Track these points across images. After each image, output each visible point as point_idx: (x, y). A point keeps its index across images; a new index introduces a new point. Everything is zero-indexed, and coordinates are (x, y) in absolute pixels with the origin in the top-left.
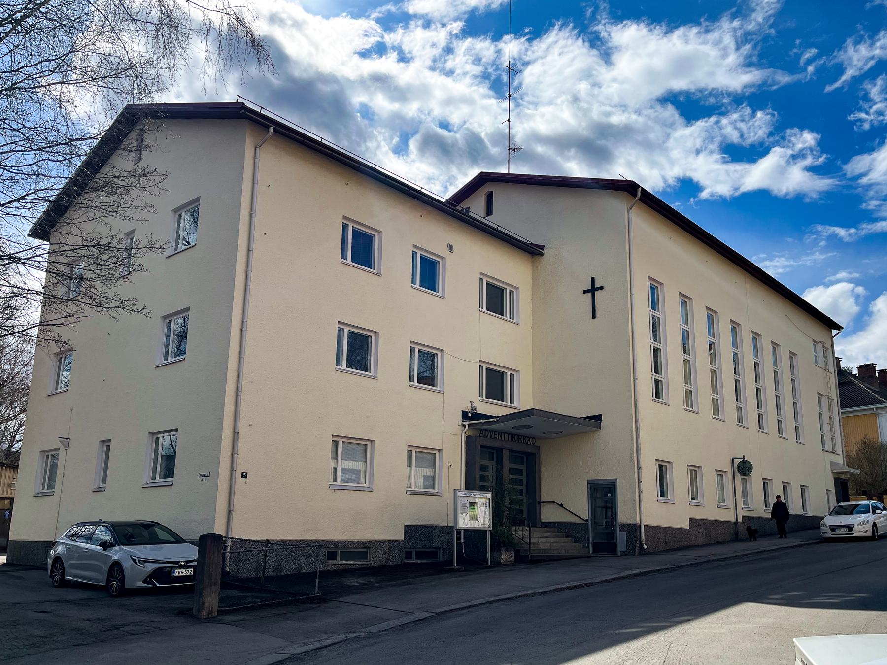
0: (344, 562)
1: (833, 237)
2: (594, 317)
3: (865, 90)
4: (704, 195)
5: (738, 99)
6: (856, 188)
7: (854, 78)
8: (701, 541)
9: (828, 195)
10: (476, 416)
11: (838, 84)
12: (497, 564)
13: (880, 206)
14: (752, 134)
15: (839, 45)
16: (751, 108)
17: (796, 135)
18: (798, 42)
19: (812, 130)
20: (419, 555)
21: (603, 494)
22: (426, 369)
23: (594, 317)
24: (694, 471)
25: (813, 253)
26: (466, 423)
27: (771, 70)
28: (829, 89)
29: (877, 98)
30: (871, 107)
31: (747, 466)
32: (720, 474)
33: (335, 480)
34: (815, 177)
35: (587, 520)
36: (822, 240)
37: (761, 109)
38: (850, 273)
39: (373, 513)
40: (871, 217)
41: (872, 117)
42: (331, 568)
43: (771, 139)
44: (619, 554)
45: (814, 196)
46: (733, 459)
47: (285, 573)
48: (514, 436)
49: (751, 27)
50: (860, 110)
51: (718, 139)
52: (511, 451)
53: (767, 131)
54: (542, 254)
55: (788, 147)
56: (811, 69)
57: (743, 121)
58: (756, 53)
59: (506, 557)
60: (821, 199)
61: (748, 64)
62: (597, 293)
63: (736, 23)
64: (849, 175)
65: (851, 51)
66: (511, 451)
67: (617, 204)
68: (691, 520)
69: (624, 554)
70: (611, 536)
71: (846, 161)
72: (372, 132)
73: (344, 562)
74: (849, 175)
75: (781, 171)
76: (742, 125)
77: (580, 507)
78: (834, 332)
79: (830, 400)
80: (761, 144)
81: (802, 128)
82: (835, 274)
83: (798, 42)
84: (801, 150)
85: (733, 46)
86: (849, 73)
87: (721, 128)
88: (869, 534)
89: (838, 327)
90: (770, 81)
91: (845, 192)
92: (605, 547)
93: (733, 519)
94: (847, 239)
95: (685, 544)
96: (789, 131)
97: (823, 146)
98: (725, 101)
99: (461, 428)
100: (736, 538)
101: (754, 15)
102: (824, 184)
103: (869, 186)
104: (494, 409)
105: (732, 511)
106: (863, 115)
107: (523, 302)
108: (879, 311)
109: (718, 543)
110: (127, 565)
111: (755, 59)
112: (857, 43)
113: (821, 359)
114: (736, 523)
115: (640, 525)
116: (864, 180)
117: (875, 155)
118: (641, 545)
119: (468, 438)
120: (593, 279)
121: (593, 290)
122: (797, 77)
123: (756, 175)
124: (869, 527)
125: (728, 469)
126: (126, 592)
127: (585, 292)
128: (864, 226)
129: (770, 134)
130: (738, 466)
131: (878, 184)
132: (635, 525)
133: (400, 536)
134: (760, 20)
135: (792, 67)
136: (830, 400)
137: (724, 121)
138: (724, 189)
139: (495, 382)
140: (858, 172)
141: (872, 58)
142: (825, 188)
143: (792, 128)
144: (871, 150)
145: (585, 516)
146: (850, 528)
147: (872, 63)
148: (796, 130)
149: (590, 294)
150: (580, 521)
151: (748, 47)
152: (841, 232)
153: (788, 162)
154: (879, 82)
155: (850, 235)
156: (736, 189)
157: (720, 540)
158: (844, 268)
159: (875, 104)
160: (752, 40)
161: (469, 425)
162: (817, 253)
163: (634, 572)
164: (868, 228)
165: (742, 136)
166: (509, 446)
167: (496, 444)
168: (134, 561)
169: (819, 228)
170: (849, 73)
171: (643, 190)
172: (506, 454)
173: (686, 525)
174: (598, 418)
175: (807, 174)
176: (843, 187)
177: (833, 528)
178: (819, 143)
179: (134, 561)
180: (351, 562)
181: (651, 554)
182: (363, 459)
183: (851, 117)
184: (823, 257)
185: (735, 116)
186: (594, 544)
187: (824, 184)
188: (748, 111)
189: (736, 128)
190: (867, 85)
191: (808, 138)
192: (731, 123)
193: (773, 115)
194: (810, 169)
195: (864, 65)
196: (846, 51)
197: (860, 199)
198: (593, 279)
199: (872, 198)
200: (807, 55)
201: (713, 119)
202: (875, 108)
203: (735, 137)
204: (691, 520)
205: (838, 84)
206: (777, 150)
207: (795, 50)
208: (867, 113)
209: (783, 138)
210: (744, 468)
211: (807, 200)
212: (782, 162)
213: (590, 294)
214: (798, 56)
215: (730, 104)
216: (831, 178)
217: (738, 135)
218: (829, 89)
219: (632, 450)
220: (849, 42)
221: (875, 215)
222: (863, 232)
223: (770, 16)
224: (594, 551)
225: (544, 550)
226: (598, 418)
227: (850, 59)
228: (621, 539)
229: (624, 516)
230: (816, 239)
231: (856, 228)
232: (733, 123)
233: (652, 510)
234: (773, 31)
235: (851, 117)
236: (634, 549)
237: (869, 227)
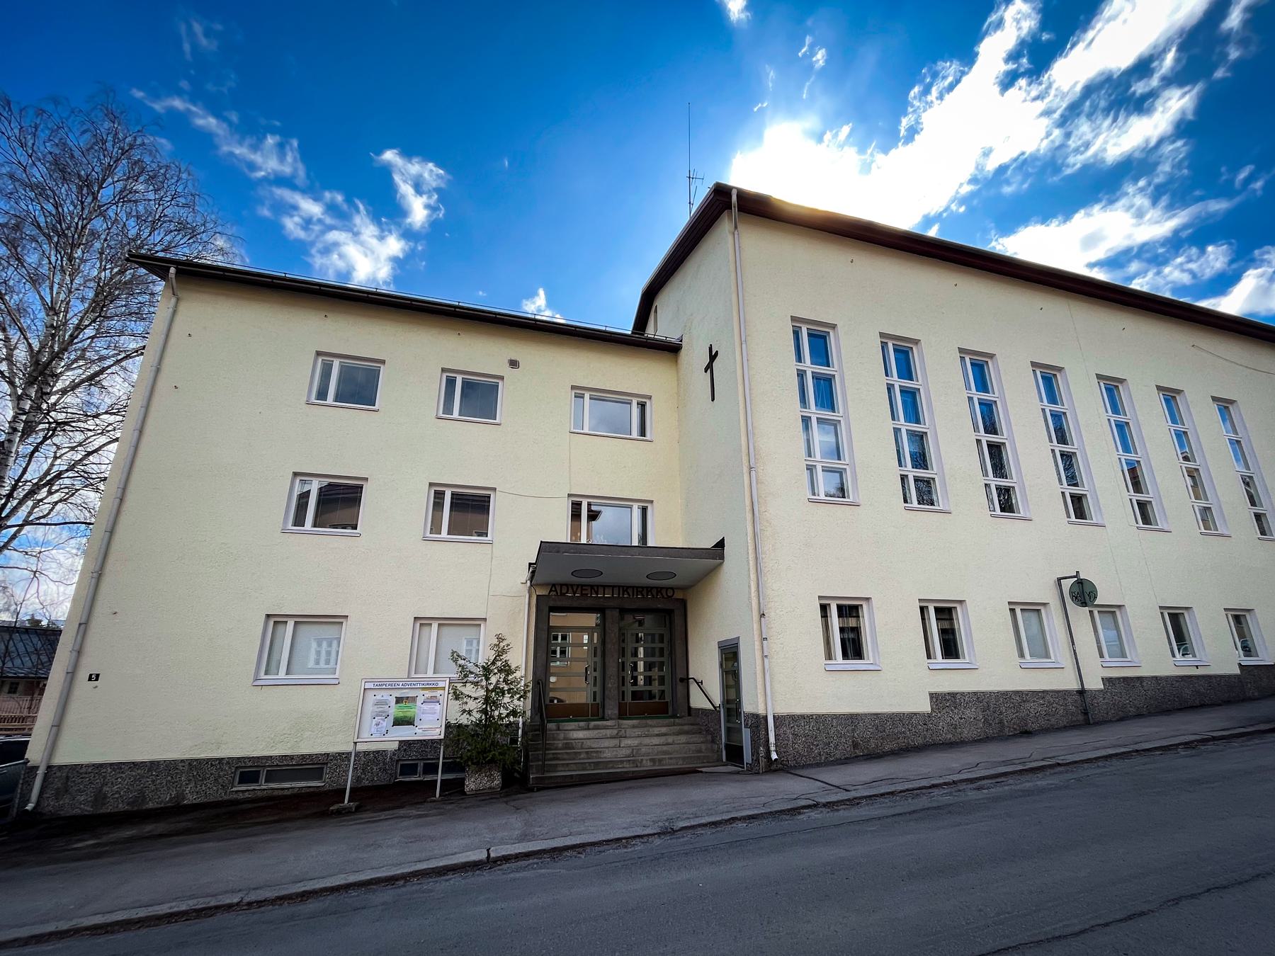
0: (243, 788)
18: (1223, 169)
31: (1087, 590)
39: (341, 711)
42: (241, 796)
46: (1059, 580)
49: (1157, 180)
68: (932, 695)
73: (243, 788)
76: (1193, 266)
93: (1075, 686)
98: (1161, 251)
109: (1027, 733)
114: (1082, 692)
115: (766, 718)
118: (768, 752)
129: (1232, 262)
137: (1167, 270)
157: (1029, 728)
173: (925, 707)
182: (328, 631)
185: (1179, 260)
200: (1243, 175)
204: (932, 695)
207: (1224, 178)
214: (1232, 181)
215: (1167, 252)
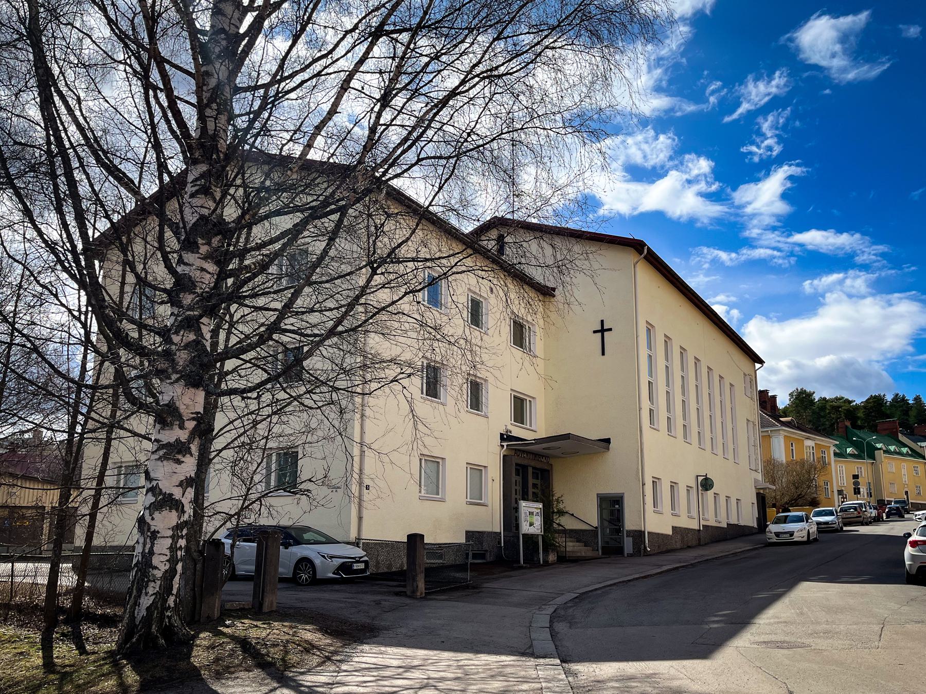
1: (715, 261)
2: (603, 354)
3: (758, 124)
4: (601, 212)
5: (644, 122)
6: (743, 216)
7: (749, 111)
8: (678, 546)
9: (718, 221)
11: (735, 116)
12: (546, 563)
13: (761, 234)
14: (654, 156)
15: (742, 81)
16: (656, 132)
17: (693, 161)
18: (706, 73)
19: (709, 157)
20: (475, 556)
21: (612, 506)
22: (476, 395)
23: (603, 354)
24: (673, 486)
25: (697, 276)
26: (505, 444)
27: (678, 98)
28: (727, 119)
29: (769, 134)
30: (762, 142)
33: (420, 492)
34: (708, 203)
36: (706, 262)
37: (664, 133)
38: (728, 296)
40: (750, 243)
41: (761, 151)
43: (671, 163)
45: (706, 221)
47: (394, 569)
48: (536, 455)
49: (664, 52)
50: (753, 143)
51: (622, 159)
52: (534, 468)
53: (668, 155)
55: (686, 172)
56: (712, 99)
57: (647, 142)
58: (666, 78)
60: (711, 224)
61: (658, 89)
63: (650, 47)
64: (736, 203)
65: (751, 86)
66: (534, 468)
67: (629, 258)
69: (630, 555)
70: (621, 541)
71: (734, 189)
74: (736, 203)
75: (676, 195)
76: (645, 147)
77: (588, 514)
78: (758, 365)
79: (754, 425)
80: (662, 167)
81: (699, 155)
82: (714, 297)
83: (706, 73)
84: (698, 176)
85: (644, 68)
86: (744, 107)
87: (626, 148)
88: (805, 539)
89: (761, 362)
90: (677, 108)
91: (732, 219)
92: (613, 551)
93: (697, 528)
94: (728, 263)
95: (669, 547)
96: (687, 157)
97: (717, 174)
99: (499, 448)
100: (699, 545)
101: (668, 41)
102: (715, 210)
103: (753, 216)
105: (696, 521)
106: (754, 149)
107: (538, 341)
108: (750, 333)
110: (318, 561)
111: (664, 84)
112: (756, 80)
113: (749, 390)
116: (749, 210)
117: (760, 185)
118: (645, 548)
119: (504, 456)
120: (602, 321)
122: (704, 106)
123: (655, 196)
124: (805, 533)
125: (693, 484)
126: (316, 582)
127: (595, 332)
128: (745, 251)
129: (671, 158)
131: (761, 214)
132: (640, 531)
133: (462, 540)
134: (674, 46)
135: (698, 97)
136: (754, 425)
137: (630, 140)
138: (623, 208)
139: (520, 407)
140: (744, 200)
141: (769, 94)
142: (715, 215)
143: (690, 153)
144: (757, 180)
145: (595, 524)
146: (791, 534)
147: (767, 99)
148: (693, 156)
149: (599, 334)
151: (659, 71)
152: (723, 256)
153: (683, 187)
154: (770, 118)
155: (731, 259)
156: (635, 209)
158: (723, 292)
159: (767, 139)
160: (664, 65)
162: (701, 276)
163: (665, 568)
164: (747, 254)
165: (645, 157)
166: (533, 463)
167: (525, 462)
168: (323, 556)
169: (705, 250)
170: (744, 107)
171: (648, 248)
172: (530, 470)
174: (608, 441)
175: (700, 199)
176: (731, 214)
177: (777, 534)
178: (714, 171)
179: (323, 556)
180: (432, 561)
181: (654, 555)
183: (744, 150)
184: (707, 279)
185: (640, 138)
186: (603, 548)
187: (715, 210)
188: (652, 133)
189: (640, 149)
190: (760, 119)
191: (703, 165)
192: (636, 144)
193: (674, 140)
194: (701, 194)
195: (760, 100)
196: (746, 86)
197: (743, 227)
198: (602, 321)
199: (754, 227)
201: (620, 138)
202: (767, 142)
203: (638, 158)
205: (735, 116)
206: (673, 174)
208: (759, 147)
209: (682, 163)
210: (706, 484)
211: (699, 225)
212: (678, 185)
213: (599, 334)
214: (705, 87)
216: (722, 205)
217: (642, 155)
218: (727, 119)
219: (638, 469)
220: (750, 77)
221: (754, 244)
222: (743, 258)
223: (682, 44)
224: (603, 553)
226: (608, 441)
227: (750, 93)
228: (628, 545)
229: (630, 524)
230: (700, 261)
231: (737, 253)
232: (637, 144)
233: (656, 519)
234: (684, 60)
235: (744, 150)
236: (639, 550)
237: (749, 252)
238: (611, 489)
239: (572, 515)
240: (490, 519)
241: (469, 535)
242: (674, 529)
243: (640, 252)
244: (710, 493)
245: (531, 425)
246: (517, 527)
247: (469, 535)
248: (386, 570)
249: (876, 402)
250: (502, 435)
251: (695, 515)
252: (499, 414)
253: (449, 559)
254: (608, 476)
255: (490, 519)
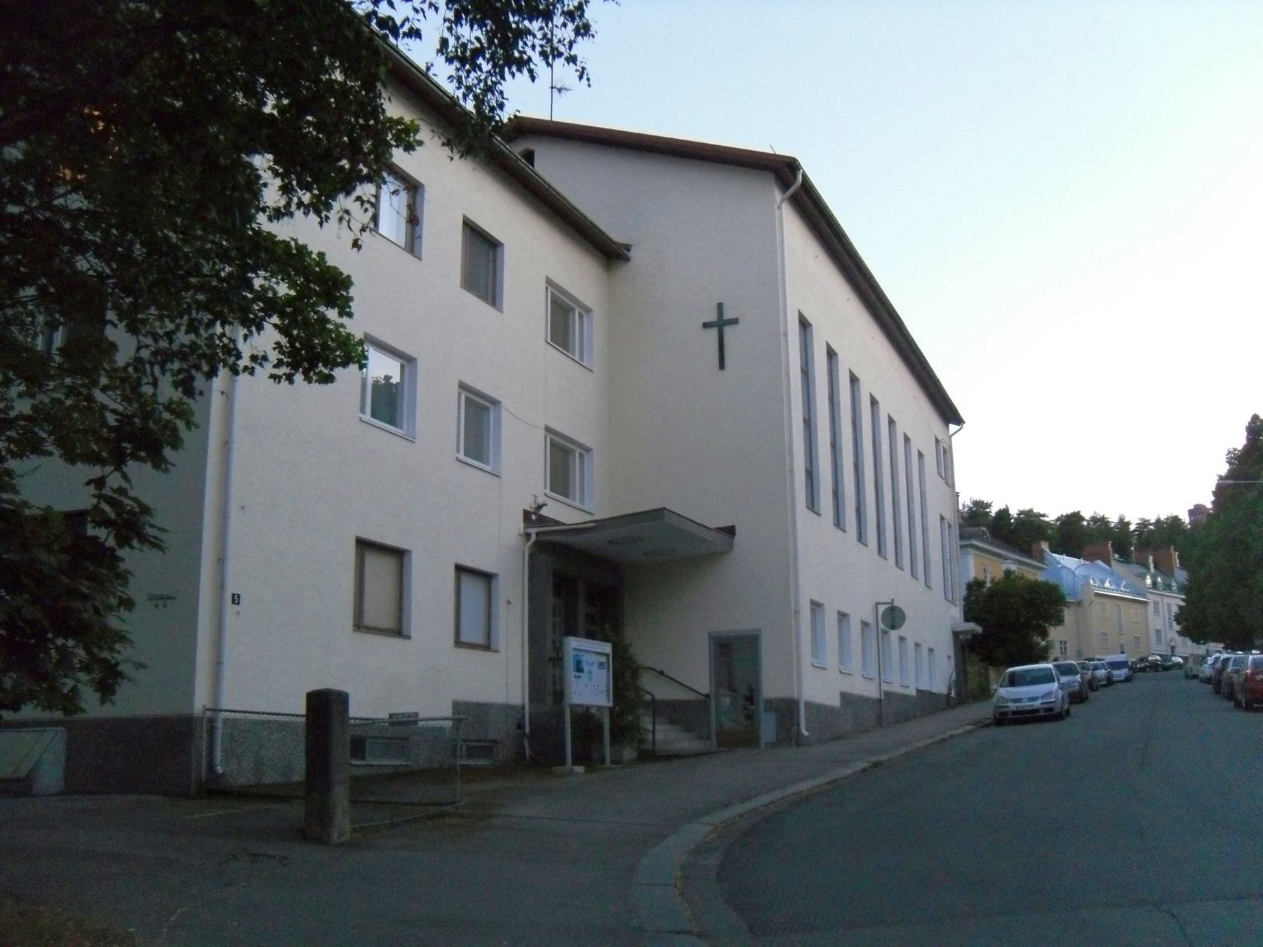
2: (722, 365)
10: (543, 520)
20: (471, 752)
21: (735, 654)
23: (722, 365)
26: (533, 531)
32: (865, 624)
35: (707, 696)
44: (763, 746)
46: (458, 643)
54: (627, 259)
59: (629, 753)
62: (728, 330)
69: (773, 745)
72: (482, 25)
77: (694, 673)
104: (561, 512)
107: (594, 333)
120: (720, 306)
121: (720, 324)
130: (884, 614)
139: (563, 457)
149: (714, 333)
150: (700, 697)
161: (537, 534)
171: (805, 176)
173: (835, 702)
186: (717, 735)
198: (720, 306)
213: (714, 333)
224: (719, 745)
225: (269, 786)
228: (768, 727)
229: (771, 688)
238: (734, 623)
239: (662, 673)
240: (501, 679)
241: (457, 706)
242: (845, 697)
243: (784, 184)
244: (894, 635)
245: (582, 501)
246: (559, 696)
247: (457, 706)
248: (278, 779)
249: (1072, 520)
250: (527, 514)
251: (874, 675)
252: (522, 476)
253: (421, 757)
254: (721, 605)
255: (501, 679)
